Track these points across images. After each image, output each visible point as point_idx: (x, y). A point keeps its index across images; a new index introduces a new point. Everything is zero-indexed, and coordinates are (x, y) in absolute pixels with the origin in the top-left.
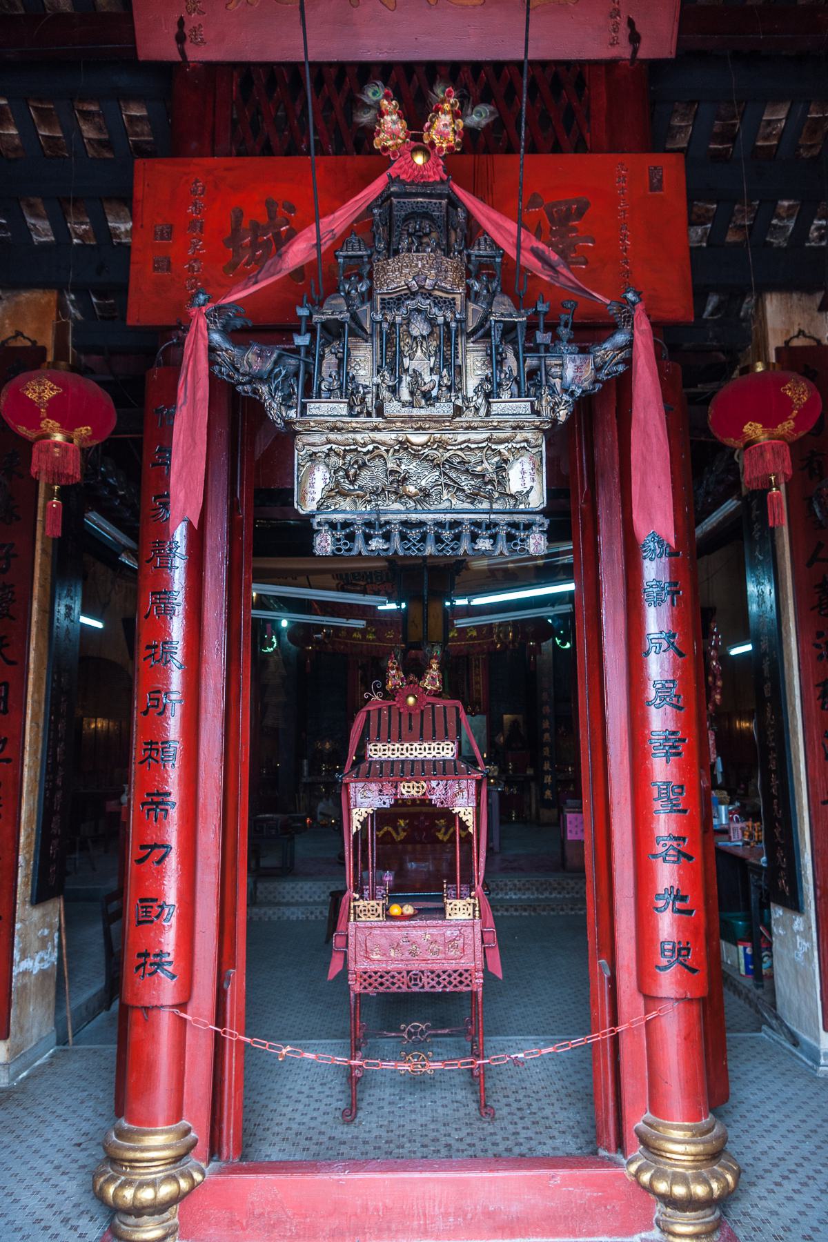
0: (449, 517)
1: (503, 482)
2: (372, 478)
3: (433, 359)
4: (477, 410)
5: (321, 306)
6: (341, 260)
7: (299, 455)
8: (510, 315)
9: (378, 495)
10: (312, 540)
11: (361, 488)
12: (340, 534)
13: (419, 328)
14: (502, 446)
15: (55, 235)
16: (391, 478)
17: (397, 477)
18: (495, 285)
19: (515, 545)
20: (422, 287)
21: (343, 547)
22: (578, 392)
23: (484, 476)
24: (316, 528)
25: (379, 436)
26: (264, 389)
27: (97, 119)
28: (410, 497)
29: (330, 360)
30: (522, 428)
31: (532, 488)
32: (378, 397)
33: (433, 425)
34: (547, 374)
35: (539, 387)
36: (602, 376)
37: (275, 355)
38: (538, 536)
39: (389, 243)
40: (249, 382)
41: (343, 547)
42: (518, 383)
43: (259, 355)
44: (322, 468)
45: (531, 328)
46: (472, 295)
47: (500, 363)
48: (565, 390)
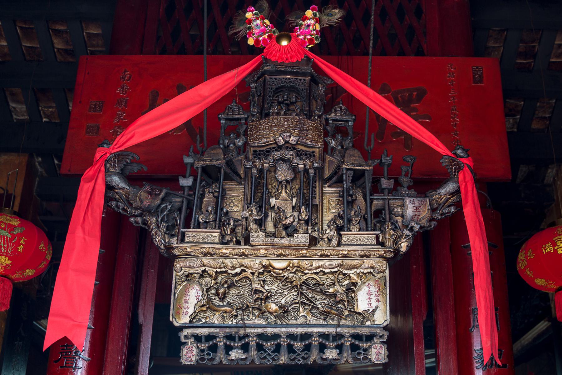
0: (300, 330)
1: (352, 301)
2: (239, 296)
3: (294, 200)
4: (330, 240)
5: (203, 154)
6: (223, 122)
7: (177, 276)
8: (360, 165)
9: (243, 311)
10: (179, 351)
11: (229, 304)
12: (204, 346)
13: (284, 173)
14: (352, 271)
15: (29, 116)
16: (255, 296)
17: (260, 295)
18: (347, 142)
19: (359, 354)
20: (287, 142)
21: (206, 357)
22: (417, 228)
23: (335, 296)
24: (183, 340)
25: (245, 261)
26: (152, 220)
27: (65, 36)
28: (271, 313)
29: (209, 198)
30: (368, 257)
31: (377, 307)
32: (246, 229)
33: (292, 252)
34: (390, 213)
35: (383, 223)
36: (437, 216)
37: (163, 194)
38: (378, 346)
39: (262, 109)
40: (141, 215)
41: (206, 357)
42: (366, 220)
43: (149, 193)
44: (196, 287)
45: (377, 173)
46: (329, 151)
47: (351, 203)
48: (406, 226)
